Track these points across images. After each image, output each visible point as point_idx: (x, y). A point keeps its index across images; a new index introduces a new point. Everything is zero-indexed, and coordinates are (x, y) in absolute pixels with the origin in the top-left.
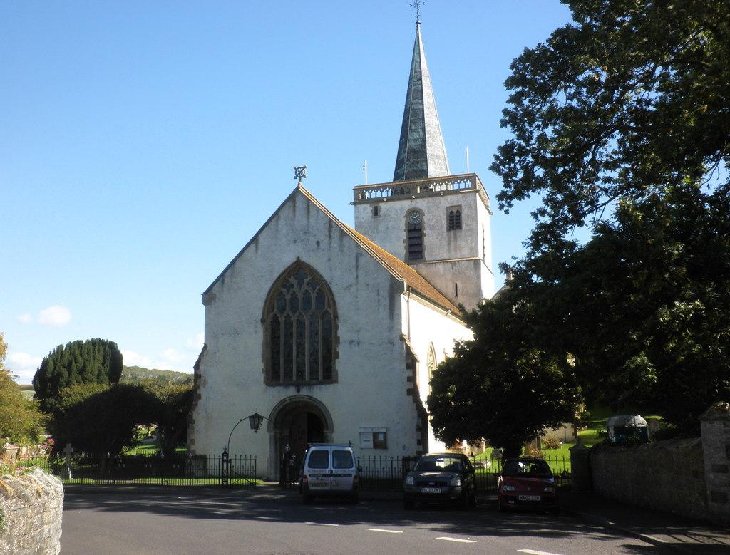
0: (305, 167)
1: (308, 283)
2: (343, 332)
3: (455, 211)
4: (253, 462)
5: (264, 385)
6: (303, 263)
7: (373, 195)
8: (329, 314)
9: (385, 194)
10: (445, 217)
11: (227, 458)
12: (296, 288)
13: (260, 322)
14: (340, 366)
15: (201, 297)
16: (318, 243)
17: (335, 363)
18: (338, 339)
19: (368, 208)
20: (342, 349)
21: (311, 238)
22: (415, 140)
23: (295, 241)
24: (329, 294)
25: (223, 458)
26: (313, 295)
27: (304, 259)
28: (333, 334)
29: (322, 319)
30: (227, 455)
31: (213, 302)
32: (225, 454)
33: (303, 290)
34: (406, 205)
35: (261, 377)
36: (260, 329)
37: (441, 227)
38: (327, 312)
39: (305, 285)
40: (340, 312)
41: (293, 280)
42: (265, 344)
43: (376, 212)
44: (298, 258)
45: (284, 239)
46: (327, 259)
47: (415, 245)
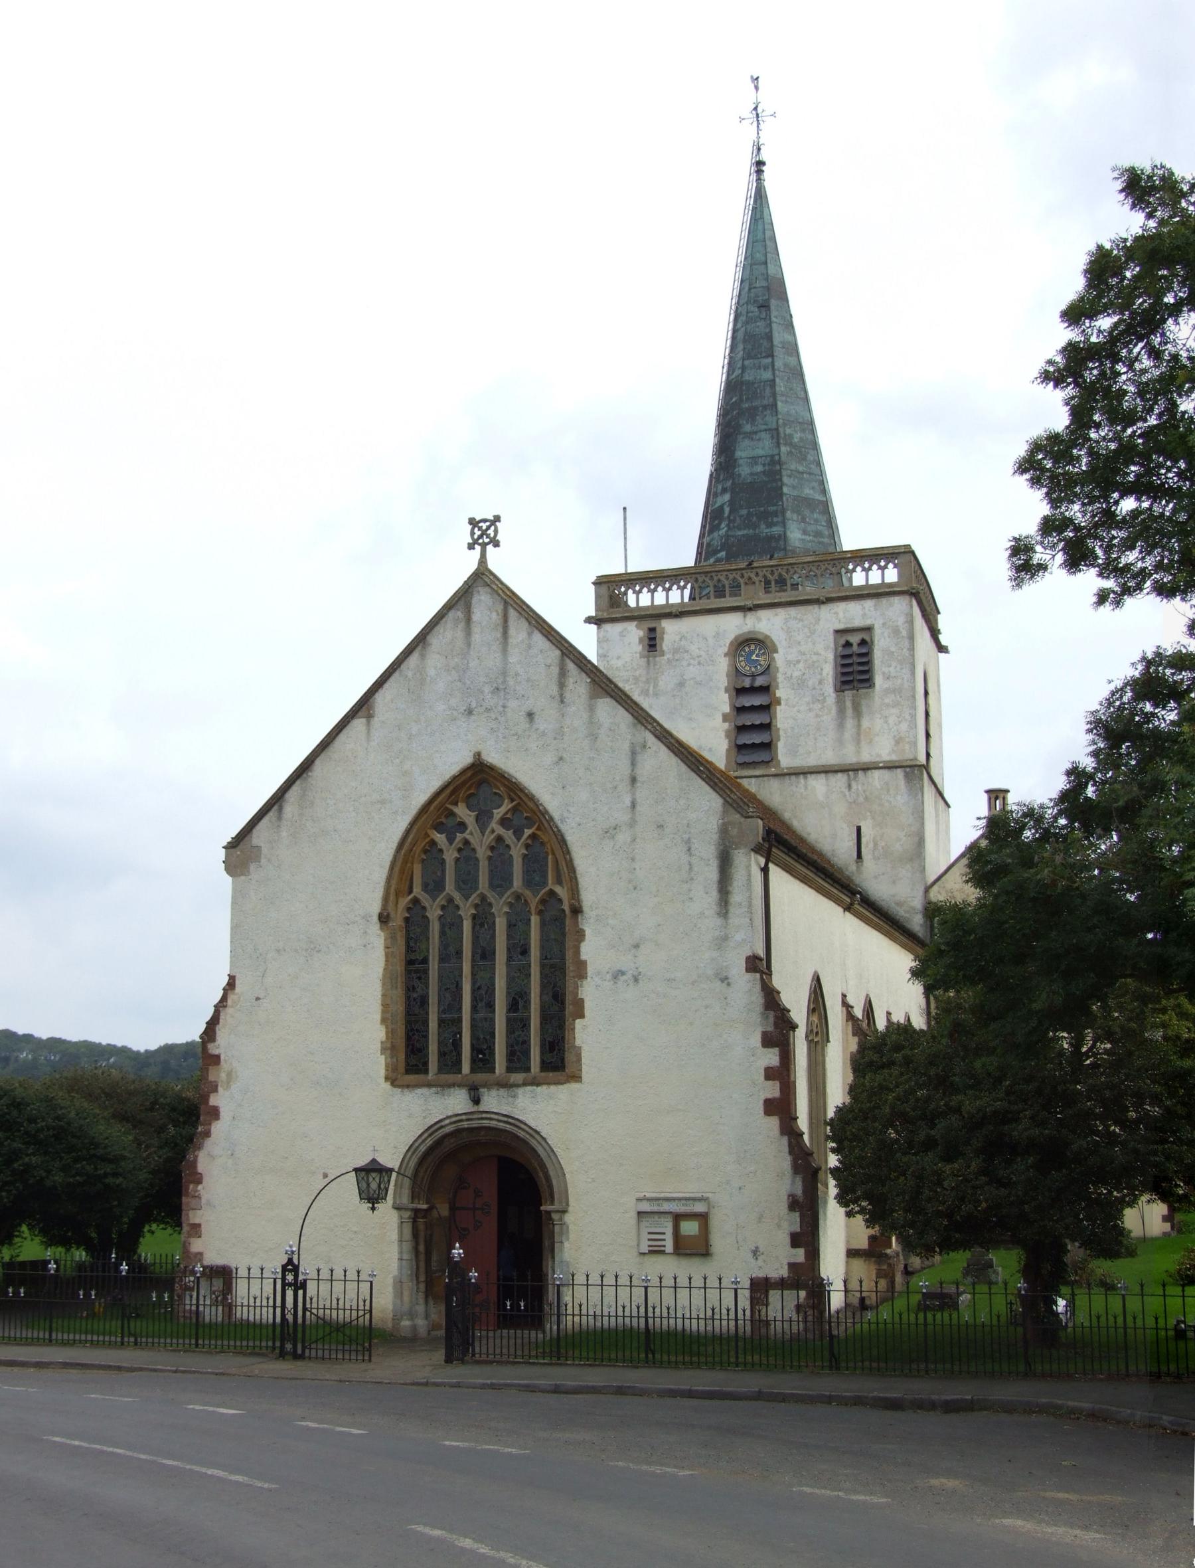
0: (497, 519)
1: (504, 822)
2: (595, 949)
3: (855, 639)
4: (365, 1287)
5: (387, 1086)
6: (492, 768)
7: (645, 600)
8: (560, 901)
9: (675, 597)
10: (830, 656)
11: (296, 1276)
12: (472, 833)
13: (375, 918)
14: (588, 1035)
15: (222, 854)
16: (530, 715)
17: (573, 1029)
18: (581, 967)
19: (634, 633)
20: (591, 992)
21: (513, 704)
22: (754, 460)
23: (470, 712)
24: (556, 846)
25: (284, 1278)
26: (517, 852)
27: (493, 757)
28: (569, 954)
29: (540, 913)
30: (296, 1269)
31: (252, 867)
32: (291, 1266)
33: (489, 839)
34: (732, 625)
35: (379, 1065)
36: (377, 939)
37: (820, 682)
38: (552, 893)
39: (493, 824)
40: (588, 898)
41: (462, 811)
42: (388, 978)
43: (652, 643)
44: (478, 754)
45: (440, 707)
46: (555, 759)
47: (753, 727)
